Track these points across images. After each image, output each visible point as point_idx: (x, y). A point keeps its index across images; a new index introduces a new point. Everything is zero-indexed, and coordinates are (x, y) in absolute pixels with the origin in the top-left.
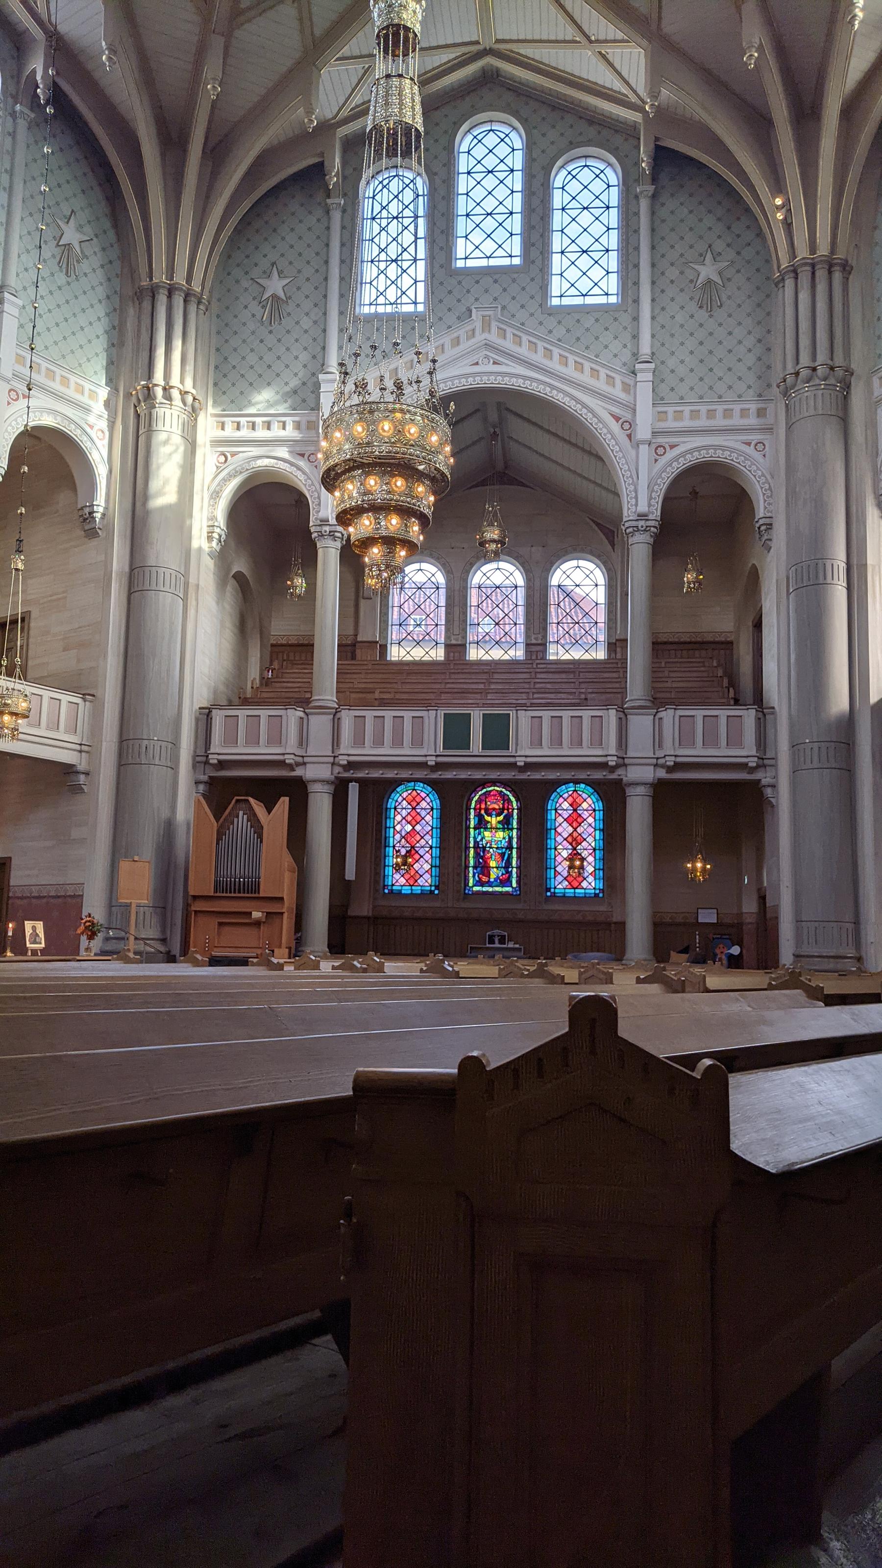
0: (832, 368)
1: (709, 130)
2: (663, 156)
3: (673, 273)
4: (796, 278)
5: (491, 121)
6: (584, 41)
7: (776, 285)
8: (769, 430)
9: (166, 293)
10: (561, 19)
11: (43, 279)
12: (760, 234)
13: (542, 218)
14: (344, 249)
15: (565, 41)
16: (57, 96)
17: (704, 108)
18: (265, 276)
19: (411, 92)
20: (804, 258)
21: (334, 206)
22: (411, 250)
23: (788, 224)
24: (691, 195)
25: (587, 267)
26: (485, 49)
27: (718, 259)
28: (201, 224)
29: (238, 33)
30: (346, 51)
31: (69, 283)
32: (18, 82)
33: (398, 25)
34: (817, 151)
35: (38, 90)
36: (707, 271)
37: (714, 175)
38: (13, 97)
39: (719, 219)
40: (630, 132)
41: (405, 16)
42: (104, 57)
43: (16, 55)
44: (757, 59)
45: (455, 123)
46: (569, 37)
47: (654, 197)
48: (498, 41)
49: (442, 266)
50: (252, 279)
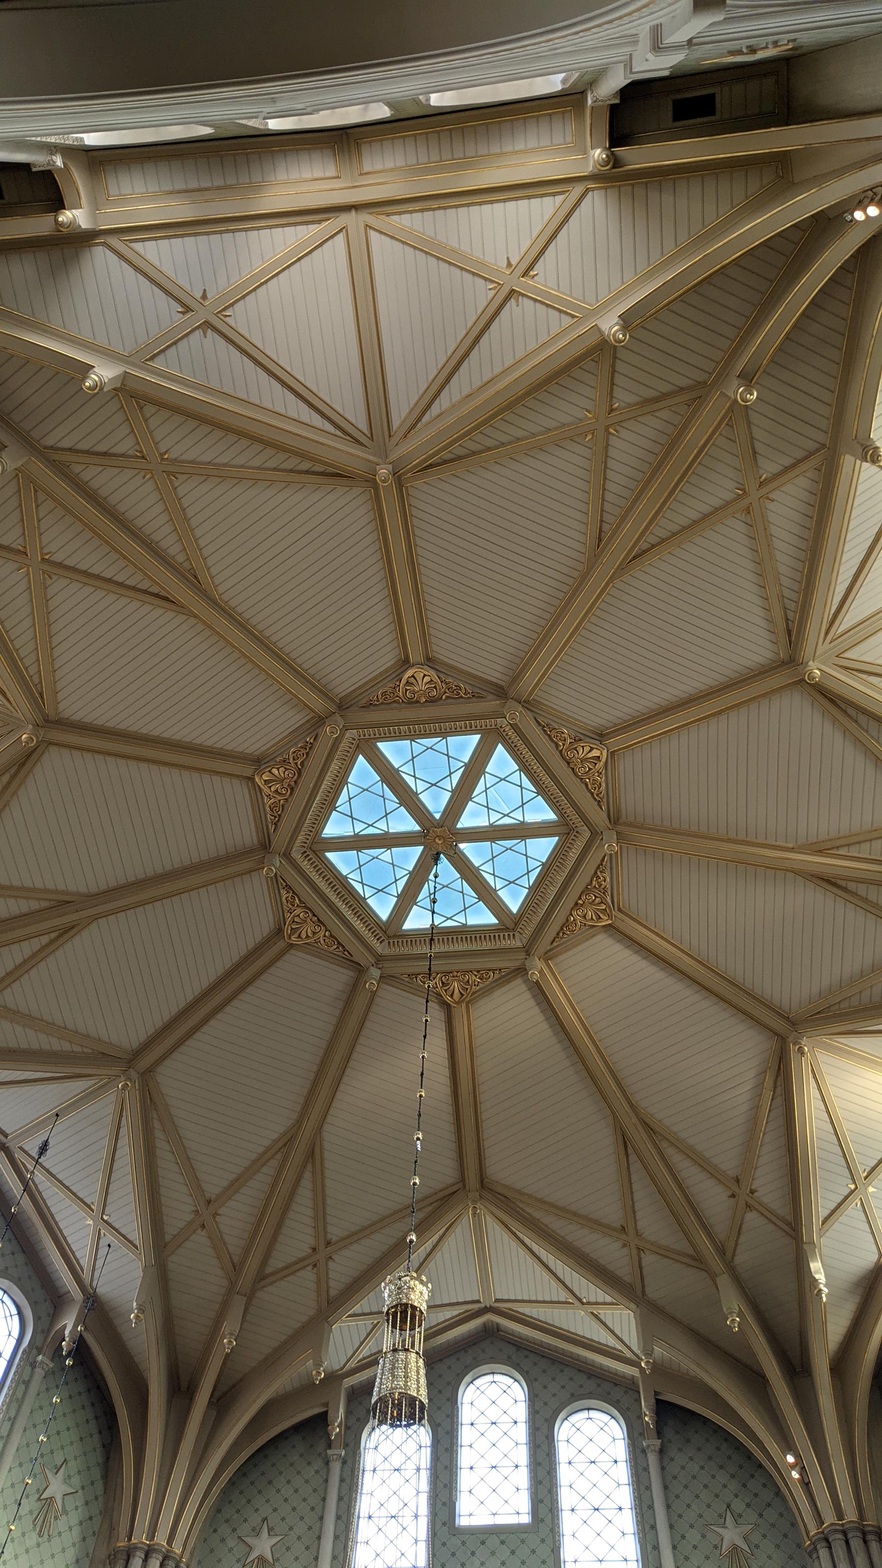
1: (706, 1385)
2: (663, 1408)
3: (693, 1536)
4: (830, 1548)
5: (493, 1373)
6: (577, 1303)
7: (810, 1555)
9: (143, 1556)
10: (554, 1284)
11: (12, 1541)
12: (778, 1493)
13: (549, 1473)
14: (344, 1484)
15: (559, 1302)
16: (81, 1349)
17: (699, 1365)
18: (254, 1533)
19: (415, 1364)
20: (832, 1524)
21: (335, 1457)
22: (413, 1481)
23: (806, 1484)
24: (699, 1449)
26: (486, 1307)
27: (740, 1521)
28: (194, 1476)
29: (259, 1294)
30: (357, 1309)
31: (38, 1545)
32: (46, 1338)
33: (406, 1305)
34: (818, 1410)
35: (64, 1343)
36: (731, 1535)
37: (718, 1429)
38: (37, 1348)
39: (733, 1476)
40: (629, 1386)
41: (412, 1296)
42: (132, 1316)
43: (52, 1312)
44: (739, 1323)
45: (458, 1375)
46: (563, 1299)
47: (662, 1451)
48: (497, 1300)
49: (444, 1524)
50: (239, 1537)
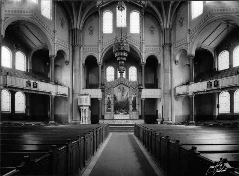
2: (145, 12)
8: (160, 51)
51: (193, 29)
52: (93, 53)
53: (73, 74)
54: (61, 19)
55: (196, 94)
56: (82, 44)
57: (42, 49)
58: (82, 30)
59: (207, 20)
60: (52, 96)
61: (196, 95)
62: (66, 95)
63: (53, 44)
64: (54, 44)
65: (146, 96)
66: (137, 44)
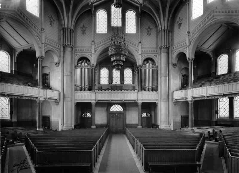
0: (165, 46)
25: (131, 27)
51: (192, 31)
52: (81, 54)
53: (65, 77)
54: (51, 16)
55: (196, 99)
56: (74, 45)
57: (28, 49)
58: (73, 30)
59: (207, 22)
60: (40, 101)
61: (195, 100)
62: (56, 100)
63: (41, 44)
64: (42, 43)
65: (142, 100)
66: (130, 44)
